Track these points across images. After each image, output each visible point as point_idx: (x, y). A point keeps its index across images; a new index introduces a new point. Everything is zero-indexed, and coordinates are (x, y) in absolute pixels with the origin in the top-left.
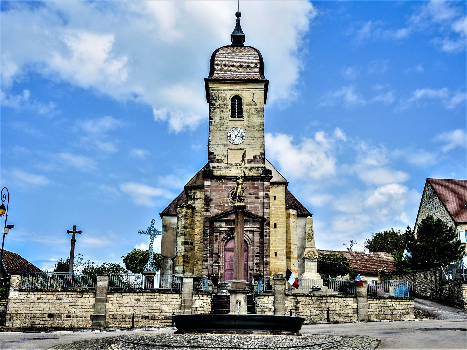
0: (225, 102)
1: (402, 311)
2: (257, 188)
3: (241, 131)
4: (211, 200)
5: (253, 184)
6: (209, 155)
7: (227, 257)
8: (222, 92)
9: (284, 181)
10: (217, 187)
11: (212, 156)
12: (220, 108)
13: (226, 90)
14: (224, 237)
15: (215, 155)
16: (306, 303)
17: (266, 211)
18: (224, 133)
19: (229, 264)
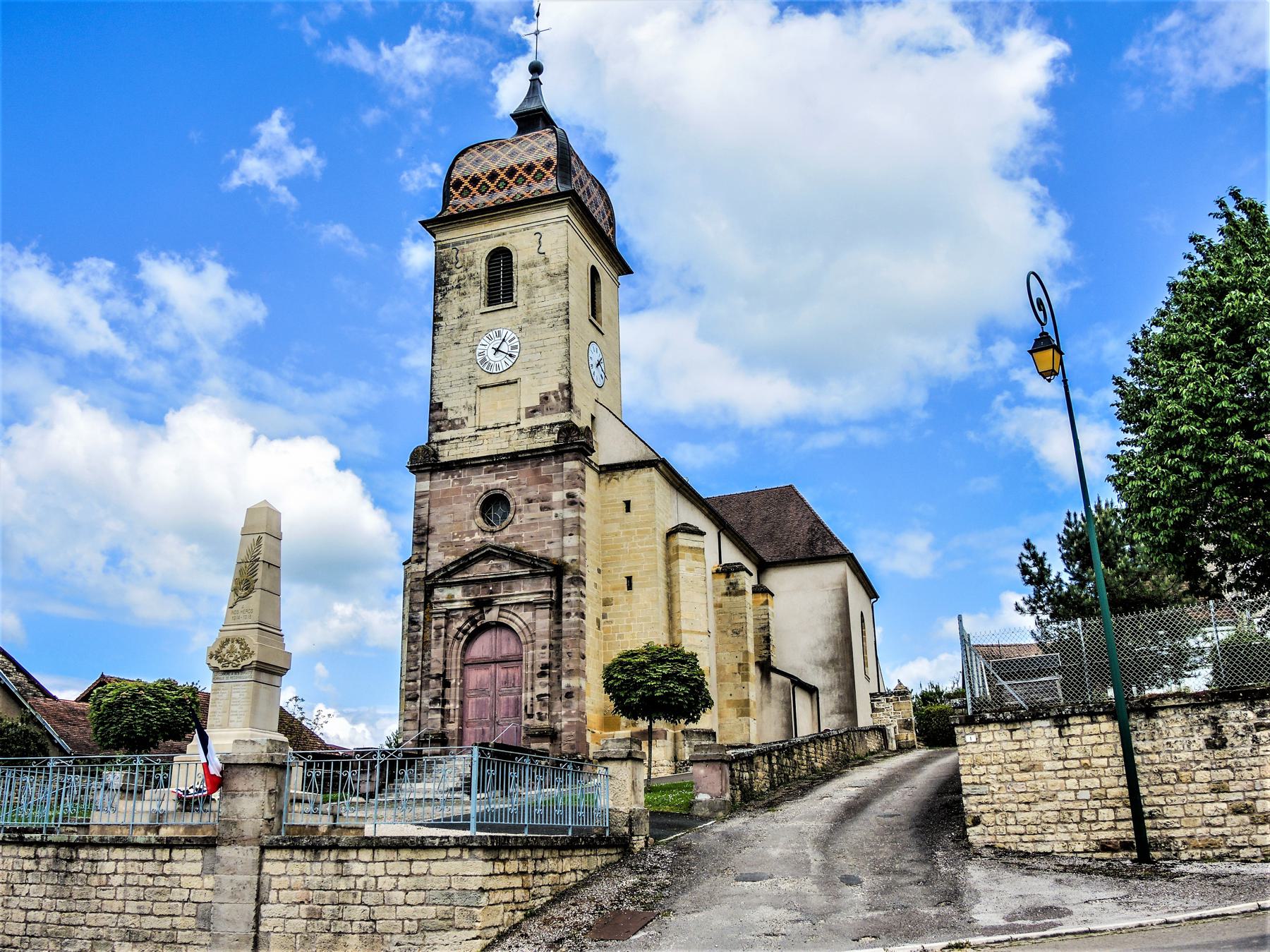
0: (472, 270)
1: (420, 912)
2: (547, 480)
3: (510, 335)
4: (429, 531)
5: (537, 472)
6: (431, 411)
7: (472, 684)
8: (465, 246)
9: (652, 456)
10: (446, 492)
11: (438, 414)
12: (458, 287)
13: (473, 240)
14: (460, 629)
15: (446, 410)
16: (16, 877)
17: (570, 541)
18: (468, 350)
19: (477, 703)
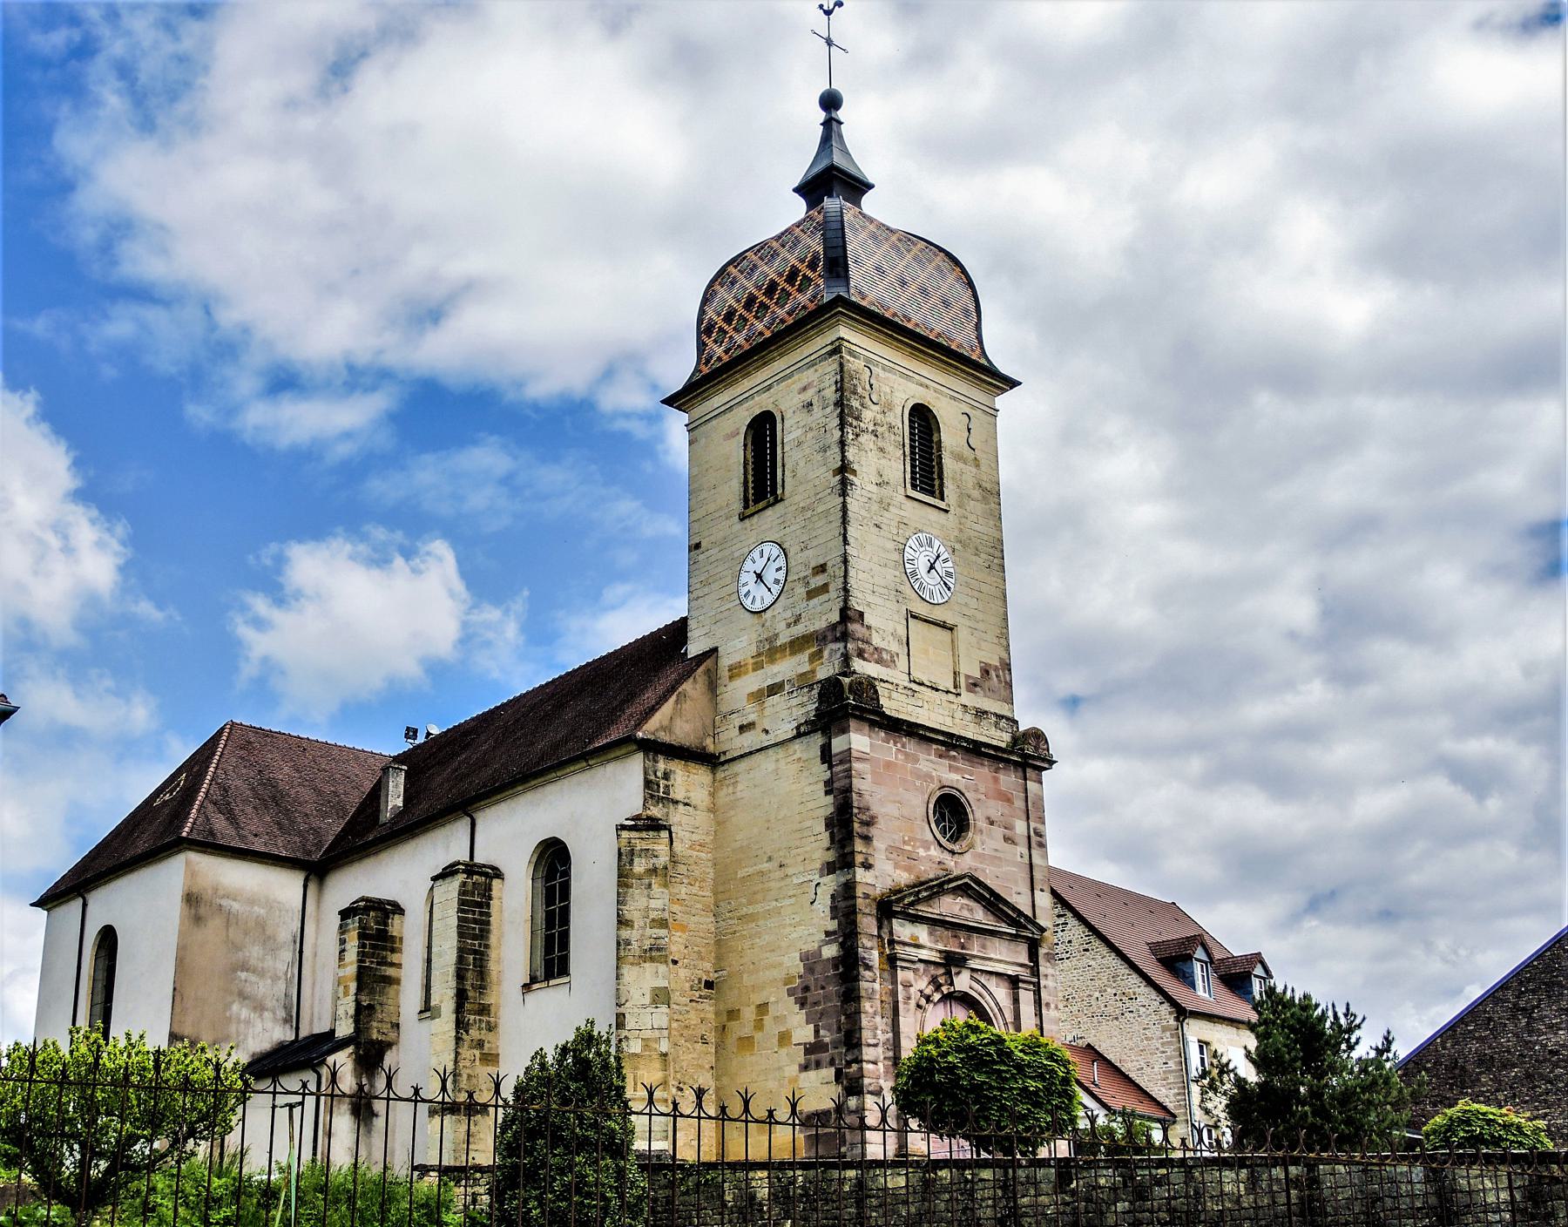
15: (869, 628)
